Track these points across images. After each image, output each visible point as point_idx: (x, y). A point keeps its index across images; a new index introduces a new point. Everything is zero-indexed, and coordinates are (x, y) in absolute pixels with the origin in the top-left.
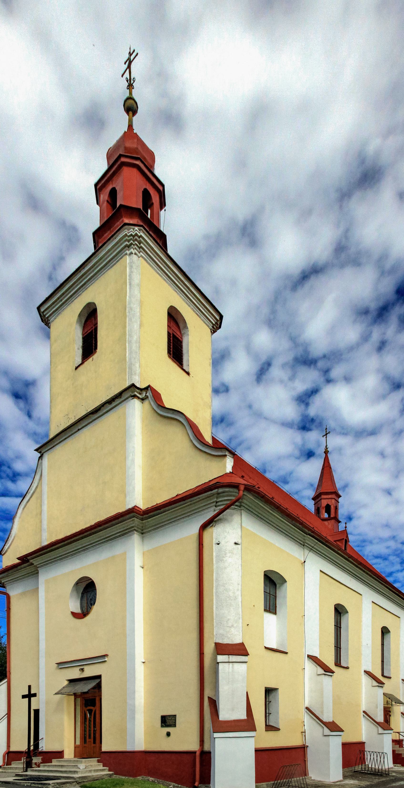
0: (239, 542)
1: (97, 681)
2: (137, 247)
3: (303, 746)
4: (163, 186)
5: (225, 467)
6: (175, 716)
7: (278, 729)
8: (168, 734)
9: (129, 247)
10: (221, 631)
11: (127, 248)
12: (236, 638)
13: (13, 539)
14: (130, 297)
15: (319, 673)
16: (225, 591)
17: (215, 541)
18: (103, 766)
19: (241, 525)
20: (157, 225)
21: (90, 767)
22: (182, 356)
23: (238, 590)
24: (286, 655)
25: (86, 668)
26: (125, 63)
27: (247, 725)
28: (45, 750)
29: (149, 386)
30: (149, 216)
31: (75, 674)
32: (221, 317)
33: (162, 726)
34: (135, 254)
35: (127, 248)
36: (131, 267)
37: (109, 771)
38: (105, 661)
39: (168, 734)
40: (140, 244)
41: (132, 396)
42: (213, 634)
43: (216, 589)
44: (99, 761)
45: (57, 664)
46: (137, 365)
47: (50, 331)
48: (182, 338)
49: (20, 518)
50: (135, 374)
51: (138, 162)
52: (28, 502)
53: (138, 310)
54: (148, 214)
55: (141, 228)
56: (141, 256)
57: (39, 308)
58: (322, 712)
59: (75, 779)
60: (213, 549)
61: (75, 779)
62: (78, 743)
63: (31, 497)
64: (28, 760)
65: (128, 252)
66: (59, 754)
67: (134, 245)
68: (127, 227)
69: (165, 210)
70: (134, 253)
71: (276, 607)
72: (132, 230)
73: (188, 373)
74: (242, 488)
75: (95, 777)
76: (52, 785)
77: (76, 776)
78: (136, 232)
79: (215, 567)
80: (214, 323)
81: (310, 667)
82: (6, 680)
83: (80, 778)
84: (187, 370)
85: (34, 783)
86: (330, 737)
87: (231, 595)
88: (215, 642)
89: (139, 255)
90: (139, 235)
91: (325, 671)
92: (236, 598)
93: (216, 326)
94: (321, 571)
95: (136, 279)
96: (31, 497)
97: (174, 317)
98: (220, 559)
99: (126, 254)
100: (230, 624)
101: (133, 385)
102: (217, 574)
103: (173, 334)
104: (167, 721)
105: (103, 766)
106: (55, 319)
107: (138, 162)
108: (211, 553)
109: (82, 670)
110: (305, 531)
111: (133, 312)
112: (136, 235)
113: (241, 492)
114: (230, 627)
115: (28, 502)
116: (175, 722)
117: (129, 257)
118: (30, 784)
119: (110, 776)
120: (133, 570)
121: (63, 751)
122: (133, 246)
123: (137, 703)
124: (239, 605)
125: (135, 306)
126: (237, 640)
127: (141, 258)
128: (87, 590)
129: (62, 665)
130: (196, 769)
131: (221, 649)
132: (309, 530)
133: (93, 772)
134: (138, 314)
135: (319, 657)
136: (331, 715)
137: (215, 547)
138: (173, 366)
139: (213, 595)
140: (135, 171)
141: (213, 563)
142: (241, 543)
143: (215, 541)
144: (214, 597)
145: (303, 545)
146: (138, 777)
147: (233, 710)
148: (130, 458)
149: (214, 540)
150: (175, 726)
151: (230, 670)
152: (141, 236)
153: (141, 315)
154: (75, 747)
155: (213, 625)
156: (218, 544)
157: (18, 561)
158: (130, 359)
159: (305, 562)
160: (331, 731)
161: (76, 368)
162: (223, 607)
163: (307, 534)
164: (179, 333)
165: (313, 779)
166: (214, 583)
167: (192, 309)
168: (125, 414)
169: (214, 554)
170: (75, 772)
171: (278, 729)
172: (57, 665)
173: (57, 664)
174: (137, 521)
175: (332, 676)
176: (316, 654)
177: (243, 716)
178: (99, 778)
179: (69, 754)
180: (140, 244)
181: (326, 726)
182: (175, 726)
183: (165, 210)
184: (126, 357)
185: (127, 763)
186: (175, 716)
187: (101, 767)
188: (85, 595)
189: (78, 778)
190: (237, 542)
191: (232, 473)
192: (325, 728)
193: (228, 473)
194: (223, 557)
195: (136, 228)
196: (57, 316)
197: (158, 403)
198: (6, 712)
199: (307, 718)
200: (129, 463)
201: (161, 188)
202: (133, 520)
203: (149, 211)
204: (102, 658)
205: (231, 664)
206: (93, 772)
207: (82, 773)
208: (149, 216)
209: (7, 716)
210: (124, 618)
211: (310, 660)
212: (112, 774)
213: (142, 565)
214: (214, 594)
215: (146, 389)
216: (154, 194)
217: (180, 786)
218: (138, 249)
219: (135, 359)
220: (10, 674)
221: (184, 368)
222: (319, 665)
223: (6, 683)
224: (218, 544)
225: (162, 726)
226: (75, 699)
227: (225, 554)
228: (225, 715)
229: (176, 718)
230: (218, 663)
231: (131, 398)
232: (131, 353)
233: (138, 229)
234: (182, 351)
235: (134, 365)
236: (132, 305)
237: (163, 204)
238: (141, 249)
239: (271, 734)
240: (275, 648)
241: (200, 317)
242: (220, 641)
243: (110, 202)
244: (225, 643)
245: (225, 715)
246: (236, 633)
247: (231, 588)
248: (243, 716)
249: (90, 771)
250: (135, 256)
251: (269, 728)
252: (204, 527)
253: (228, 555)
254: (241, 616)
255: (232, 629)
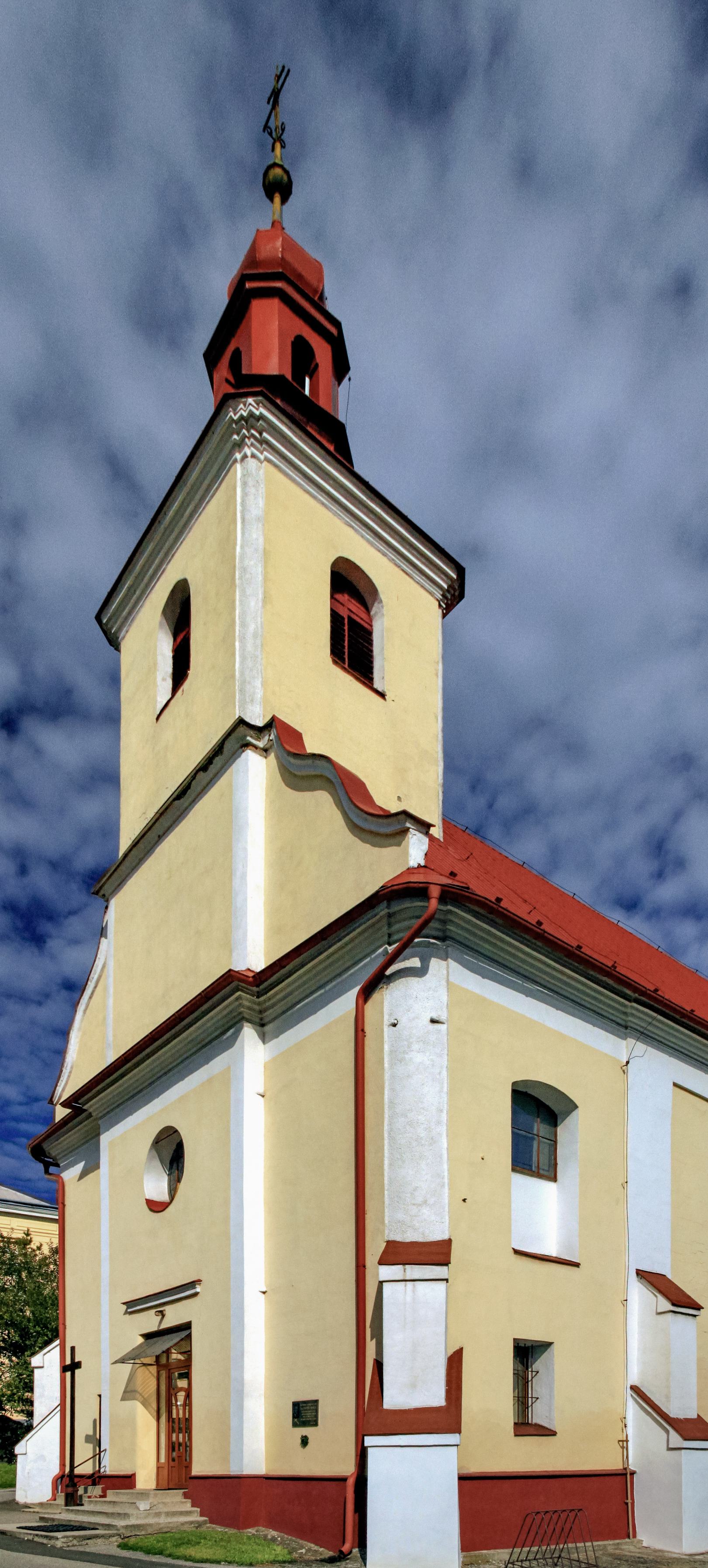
0: (443, 1017)
1: (183, 1334)
2: (255, 442)
3: (624, 1472)
4: (337, 324)
5: (406, 854)
6: (316, 1401)
7: (554, 1434)
8: (305, 1441)
9: (240, 445)
10: (400, 1216)
11: (237, 449)
12: (432, 1230)
13: (70, 1072)
14: (242, 547)
15: (659, 1311)
16: (408, 1127)
17: (387, 1020)
18: (193, 1506)
19: (448, 981)
20: (333, 414)
21: (161, 1506)
22: (372, 662)
23: (439, 1123)
24: (576, 1268)
25: (168, 1309)
26: (268, 103)
27: (445, 1419)
28: (108, 1473)
29: (274, 719)
30: (307, 392)
31: (150, 1322)
32: (461, 571)
33: (295, 1425)
34: (253, 456)
35: (237, 449)
36: (245, 484)
37: (201, 1515)
38: (196, 1294)
39: (305, 1441)
40: (261, 434)
41: (242, 747)
42: (383, 1222)
43: (390, 1124)
44: (186, 1496)
45: (124, 1303)
46: (258, 683)
47: (119, 658)
48: (371, 626)
49: (79, 1029)
50: (252, 701)
51: (278, 284)
52: (90, 998)
53: (260, 570)
54: (304, 388)
55: (260, 398)
56: (267, 460)
57: (98, 618)
58: (668, 1397)
59: (118, 1530)
60: (383, 1037)
61: (118, 1530)
62: (163, 1459)
63: (95, 987)
64: (70, 1490)
65: (238, 456)
66: (127, 1481)
67: (249, 438)
68: (231, 402)
69: (350, 379)
70: (249, 454)
71: (556, 1164)
72: (242, 406)
73: (382, 695)
74: (435, 892)
75: (162, 1526)
76: (63, 1540)
77: (120, 1523)
78: (251, 407)
79: (387, 1076)
80: (445, 586)
81: (640, 1296)
82: (58, 1342)
83: (127, 1527)
84: (380, 690)
85: (37, 1535)
86: (683, 1451)
87: (422, 1135)
88: (386, 1239)
89: (262, 457)
90: (257, 413)
91: (674, 1305)
92: (433, 1141)
93: (452, 598)
94: (675, 1085)
95: (257, 505)
96: (95, 987)
97: (347, 582)
98: (398, 1058)
99: (236, 461)
100: (419, 1200)
101: (241, 722)
102: (392, 1090)
103: (349, 617)
104: (304, 1413)
105: (193, 1506)
106: (127, 632)
107: (278, 284)
108: (383, 1044)
109: (162, 1314)
110: (626, 994)
111: (248, 576)
112: (251, 415)
113: (434, 903)
114: (420, 1205)
115: (90, 998)
116: (316, 1416)
117: (242, 466)
118: (30, 1537)
119: (199, 1525)
120: (240, 1102)
121: (134, 1475)
122: (247, 440)
123: (248, 1376)
124: (441, 1157)
125: (252, 563)
126: (436, 1233)
127: (265, 463)
128: (171, 1151)
129: (133, 1306)
130: (330, 1513)
131: (397, 1253)
132: (635, 990)
133: (163, 1516)
134: (260, 578)
135: (669, 1277)
136: (694, 1404)
137: (387, 1030)
138: (346, 683)
139: (383, 1139)
140: (275, 304)
141: (383, 1068)
142: (447, 1021)
143: (387, 1020)
144: (386, 1142)
145: (622, 1027)
146: (250, 1530)
147: (413, 1386)
148: (238, 874)
149: (386, 1017)
150: (316, 1424)
151: (409, 1299)
152: (262, 417)
153: (266, 579)
154: (158, 1468)
155: (384, 1203)
156: (394, 1025)
157: (374, 1340)
158: (242, 673)
159: (628, 1063)
160: (685, 1440)
161: (158, 718)
162: (404, 1162)
163: (630, 1001)
164: (364, 615)
165: (645, 1544)
166: (386, 1110)
167: (392, 560)
168: (230, 785)
169: (386, 1048)
170: (126, 1516)
171: (554, 1434)
172: (125, 1307)
173: (124, 1303)
174: (245, 999)
175: (695, 1316)
176: (662, 1266)
177: (436, 1397)
178: (172, 1528)
179: (146, 1479)
180: (261, 434)
181: (673, 1427)
182: (316, 1424)
183: (350, 379)
184: (235, 670)
185: (230, 1499)
186: (316, 1401)
187: (187, 1506)
188: (175, 1165)
189: (123, 1527)
190: (435, 1017)
191: (425, 867)
192: (672, 1432)
193: (414, 868)
194: (405, 1052)
195: (250, 400)
196: (130, 625)
197: (288, 747)
198: (59, 1402)
199: (633, 1410)
200: (236, 882)
201: (334, 331)
202: (237, 999)
203: (307, 380)
204: (186, 1290)
205: (409, 1284)
206: (163, 1516)
207: (137, 1518)
208: (307, 392)
209: (59, 1408)
210: (227, 1202)
211: (643, 1281)
212: (205, 1522)
213: (261, 1091)
214: (386, 1135)
215: (269, 726)
216: (322, 345)
217: (322, 1549)
218: (258, 445)
219: (251, 670)
220: (65, 1328)
221: (375, 686)
222: (660, 1292)
223: (58, 1348)
224: (394, 1025)
225: (295, 1425)
226: (158, 1372)
227: (409, 1047)
228: (397, 1396)
229: (317, 1406)
230: (381, 1283)
231: (241, 750)
232: (243, 658)
233: (254, 401)
234: (372, 651)
235: (249, 683)
236: (246, 562)
237: (341, 368)
238: (264, 446)
239: (530, 1443)
240: (554, 1255)
241: (412, 577)
242: (398, 1238)
243: (233, 381)
244: (408, 1240)
245: (397, 1396)
246: (433, 1218)
247: (422, 1118)
248: (436, 1397)
249: (158, 1514)
250: (253, 460)
251: (525, 1427)
252: (367, 992)
253: (415, 1047)
254: (446, 1180)
255: (425, 1211)
